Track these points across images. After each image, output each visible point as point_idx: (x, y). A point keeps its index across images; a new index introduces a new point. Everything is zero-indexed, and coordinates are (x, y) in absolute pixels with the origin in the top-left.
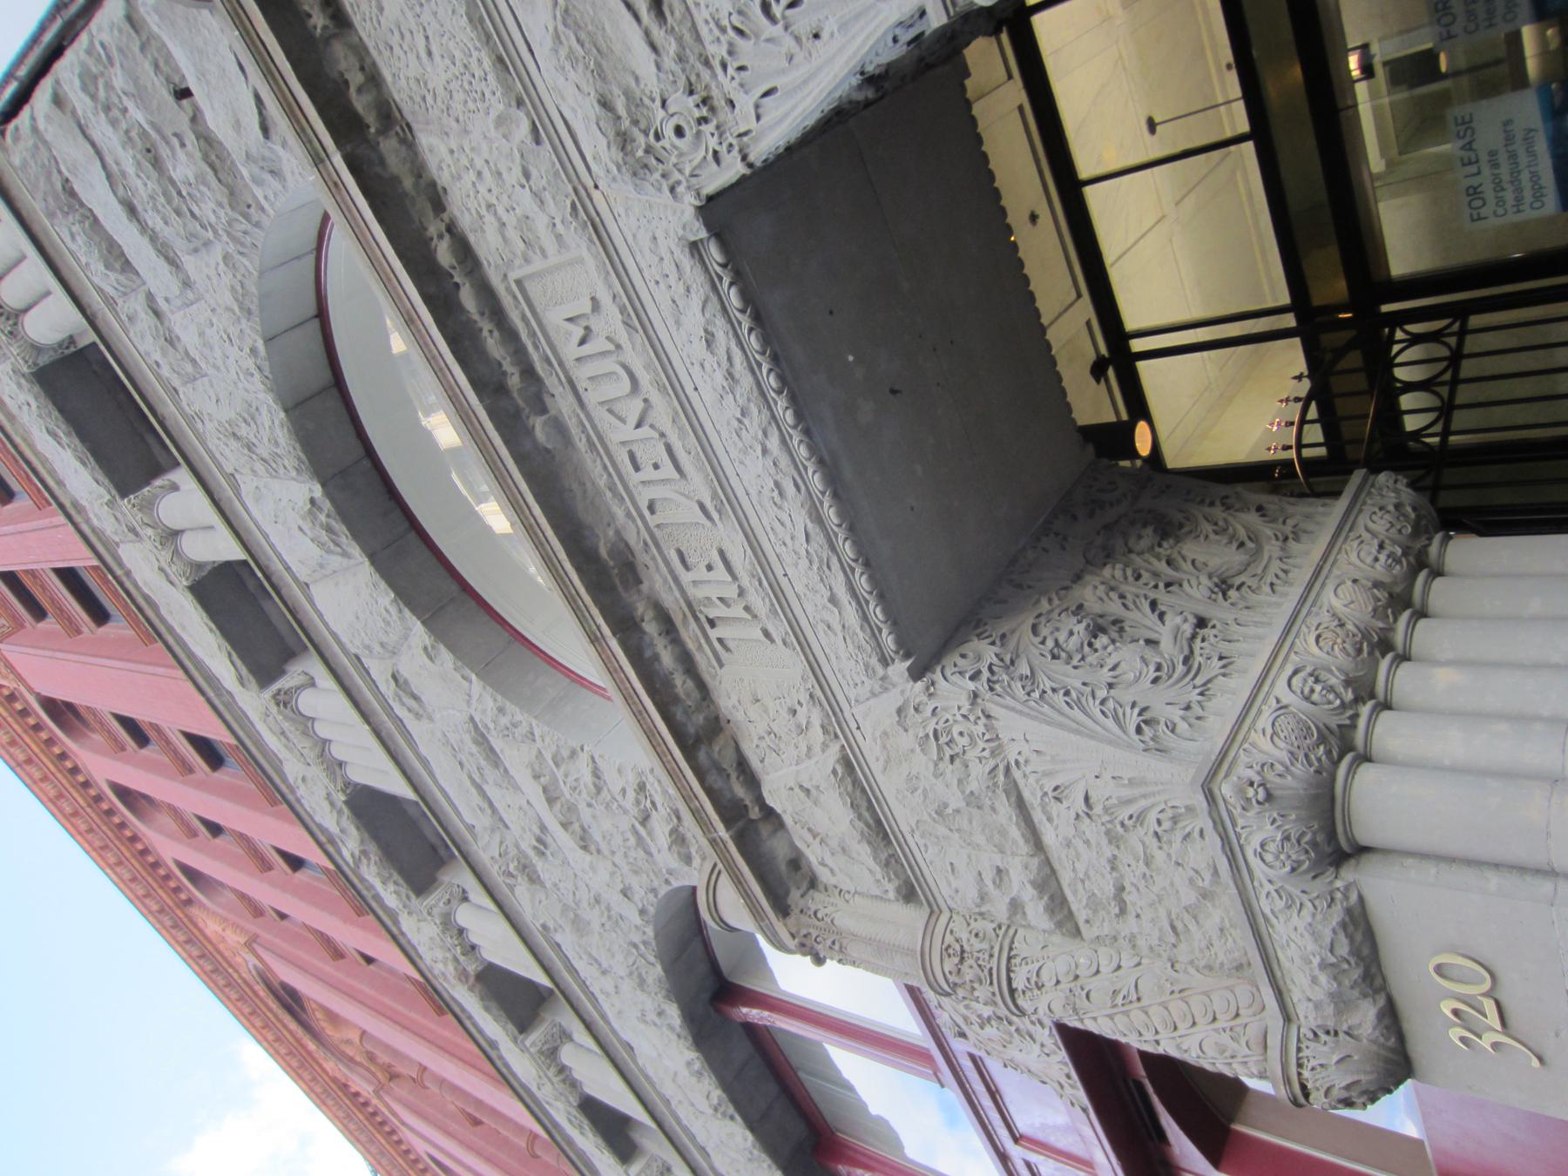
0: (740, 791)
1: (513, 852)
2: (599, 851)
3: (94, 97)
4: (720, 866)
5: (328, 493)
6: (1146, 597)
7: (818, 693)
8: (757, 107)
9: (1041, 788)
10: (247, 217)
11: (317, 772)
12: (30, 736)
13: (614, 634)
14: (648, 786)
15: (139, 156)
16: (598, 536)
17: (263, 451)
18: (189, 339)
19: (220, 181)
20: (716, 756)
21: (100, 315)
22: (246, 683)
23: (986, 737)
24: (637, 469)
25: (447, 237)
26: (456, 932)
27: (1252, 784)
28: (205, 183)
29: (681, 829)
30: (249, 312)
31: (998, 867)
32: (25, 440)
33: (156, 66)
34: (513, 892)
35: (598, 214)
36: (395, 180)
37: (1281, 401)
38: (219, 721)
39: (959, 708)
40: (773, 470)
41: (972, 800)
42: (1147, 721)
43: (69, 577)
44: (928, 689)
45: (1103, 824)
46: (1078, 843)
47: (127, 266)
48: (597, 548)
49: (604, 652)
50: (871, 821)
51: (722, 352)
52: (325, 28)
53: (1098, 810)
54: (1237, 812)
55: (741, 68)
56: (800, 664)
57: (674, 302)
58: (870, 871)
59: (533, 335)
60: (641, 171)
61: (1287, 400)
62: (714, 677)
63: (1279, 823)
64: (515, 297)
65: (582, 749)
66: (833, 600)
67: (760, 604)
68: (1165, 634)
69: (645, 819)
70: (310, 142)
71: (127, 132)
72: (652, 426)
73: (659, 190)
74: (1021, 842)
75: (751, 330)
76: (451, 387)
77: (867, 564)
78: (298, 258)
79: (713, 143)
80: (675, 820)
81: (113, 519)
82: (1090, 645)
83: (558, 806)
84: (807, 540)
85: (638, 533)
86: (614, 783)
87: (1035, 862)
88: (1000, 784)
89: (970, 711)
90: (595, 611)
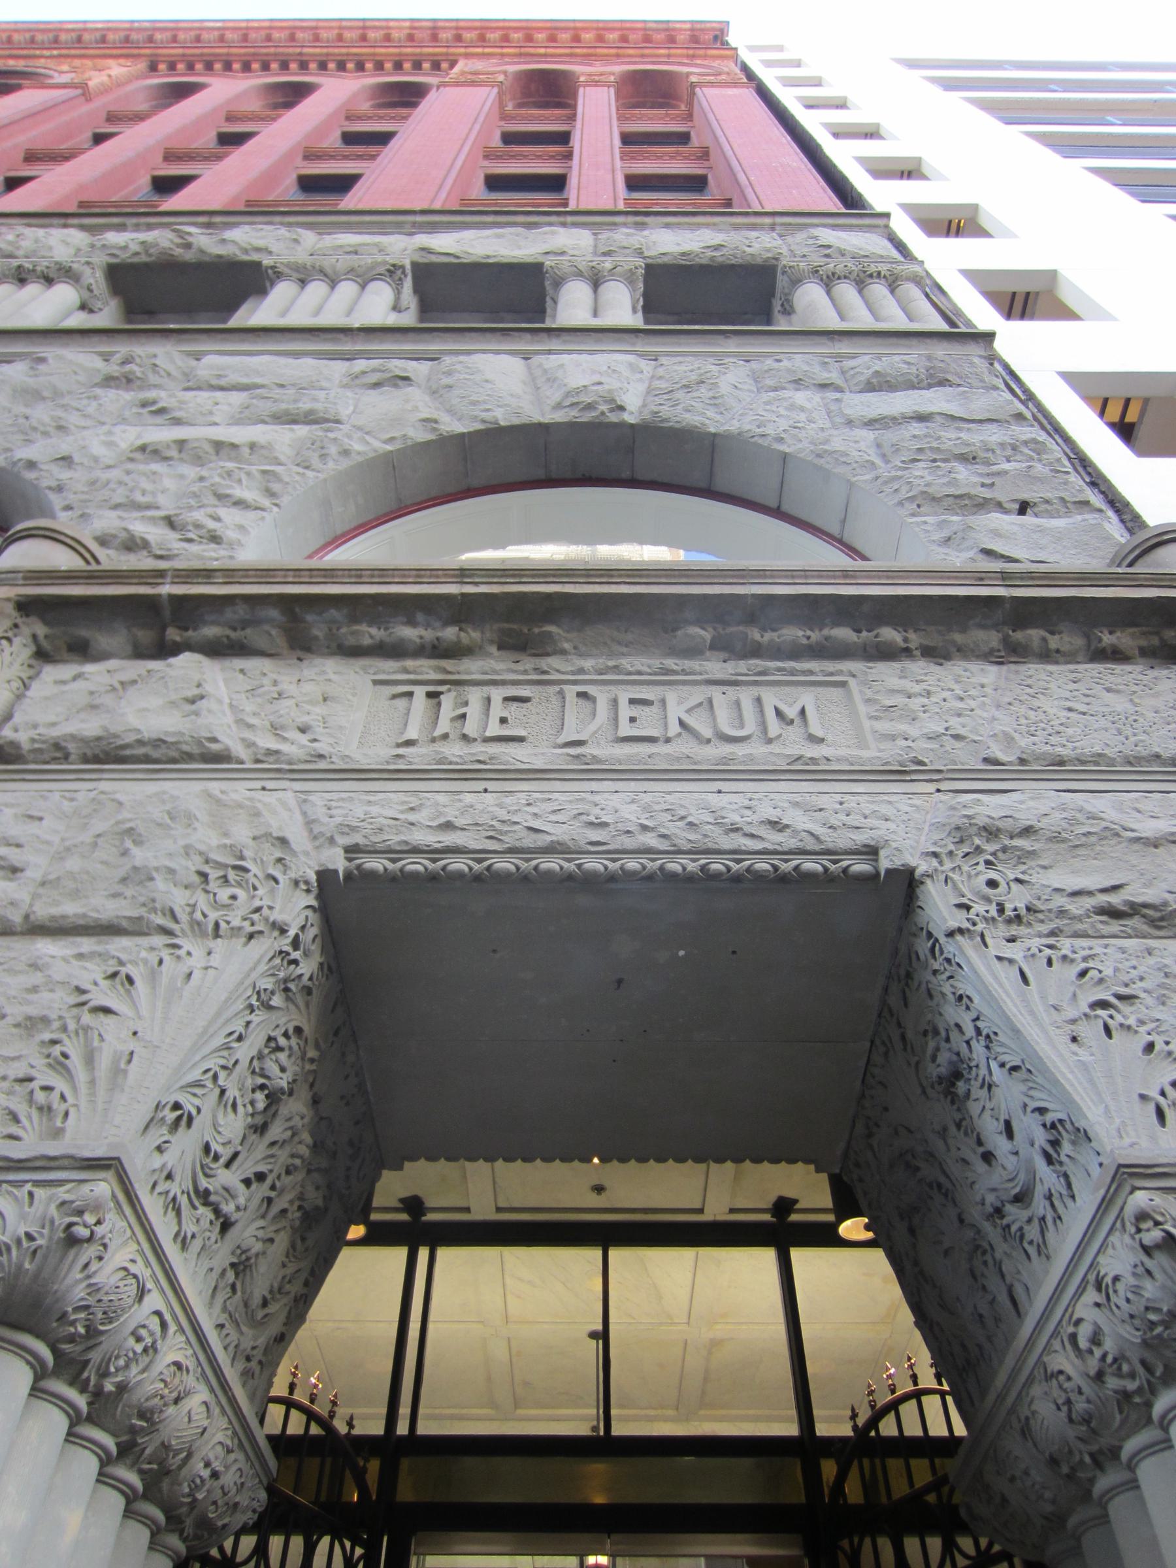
0: (210, 631)
1: (153, 379)
2: (131, 460)
3: (1026, 443)
4: (94, 567)
5: (622, 425)
6: (271, 1171)
7: (322, 765)
8: (1011, 961)
9: (135, 963)
10: (911, 499)
11: (300, 256)
12: (320, 55)
13: (463, 595)
14: (213, 546)
15: (973, 448)
16: (568, 632)
17: (680, 395)
18: (801, 397)
19: (948, 496)
20: (266, 627)
21: (830, 344)
22: (423, 253)
23: (223, 925)
24: (632, 701)
25: (904, 645)
26: (51, 275)
27: (99, 1222)
28: (949, 484)
29: (145, 553)
30: (819, 456)
31: (22, 870)
32: (714, 224)
33: (1047, 502)
34: (100, 354)
35: (912, 781)
36: (964, 630)
37: (335, 1396)
38: (388, 206)
39: (270, 908)
40: (620, 826)
41: (141, 876)
42: (183, 1119)
43: (344, 183)
44: (307, 882)
45: (60, 1018)
46: (37, 978)
47: (871, 387)
48: (559, 626)
49: (446, 576)
50: (128, 752)
51: (762, 831)
52: (1100, 640)
53: (87, 1018)
54: (62, 1193)
55: (1050, 963)
56: (363, 760)
57: (821, 810)
58: (54, 724)
59: (793, 672)
60: (958, 835)
61: (334, 1403)
62: (365, 669)
63: (25, 1244)
64: (831, 674)
65: (276, 505)
66: (448, 826)
67: (454, 751)
68: (229, 1178)
69: (170, 522)
70: (1022, 579)
71: (993, 451)
72: (679, 735)
73: (935, 843)
74: (55, 911)
75: (776, 868)
76: (772, 577)
77: (478, 878)
78: (844, 521)
79: (979, 908)
80: (159, 552)
81: (625, 244)
82: (262, 1087)
83: (208, 448)
84: (530, 829)
85: (558, 671)
86: (229, 515)
87: (16, 917)
88: (153, 916)
89: (266, 920)
90: (495, 589)
